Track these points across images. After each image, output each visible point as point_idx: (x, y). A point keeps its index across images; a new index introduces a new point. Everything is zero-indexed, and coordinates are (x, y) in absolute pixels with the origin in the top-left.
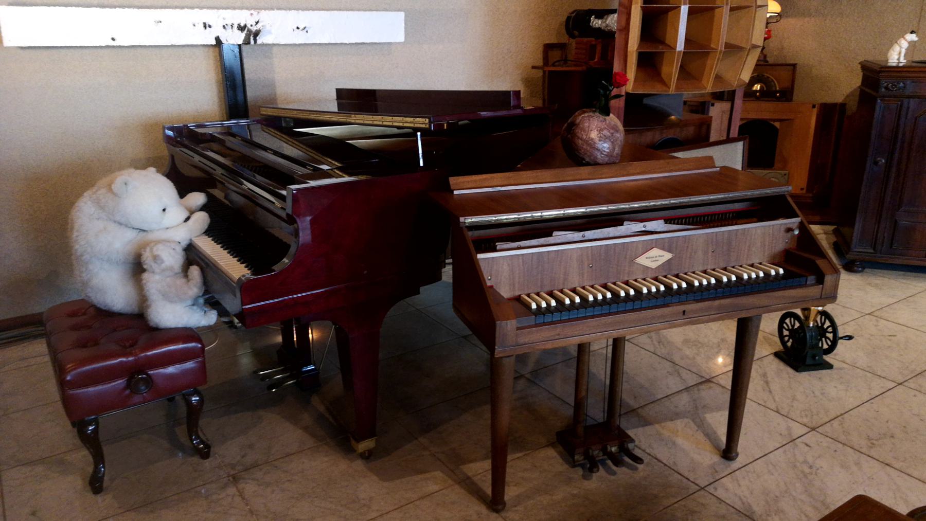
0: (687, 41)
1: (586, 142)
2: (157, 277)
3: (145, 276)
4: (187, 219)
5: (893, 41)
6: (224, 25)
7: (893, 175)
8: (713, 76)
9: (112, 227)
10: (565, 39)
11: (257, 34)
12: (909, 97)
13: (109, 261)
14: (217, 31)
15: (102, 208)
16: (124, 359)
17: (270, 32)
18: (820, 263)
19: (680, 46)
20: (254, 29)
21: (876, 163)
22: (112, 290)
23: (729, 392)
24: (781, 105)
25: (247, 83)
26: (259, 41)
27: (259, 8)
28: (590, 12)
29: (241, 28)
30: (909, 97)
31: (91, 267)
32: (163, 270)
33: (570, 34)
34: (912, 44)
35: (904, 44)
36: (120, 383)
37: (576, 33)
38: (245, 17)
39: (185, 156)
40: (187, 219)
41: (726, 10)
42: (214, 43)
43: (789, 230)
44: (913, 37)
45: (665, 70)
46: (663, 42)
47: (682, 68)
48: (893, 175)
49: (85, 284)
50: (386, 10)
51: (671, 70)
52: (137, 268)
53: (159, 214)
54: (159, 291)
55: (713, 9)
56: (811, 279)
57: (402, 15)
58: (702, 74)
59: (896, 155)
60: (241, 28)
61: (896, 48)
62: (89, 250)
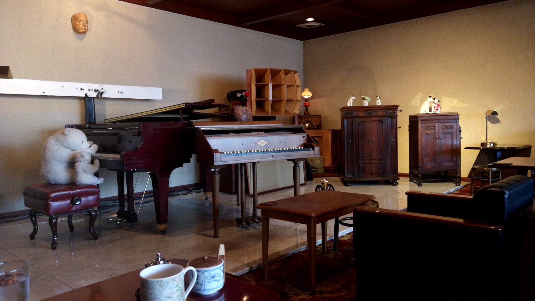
0: (273, 97)
1: (238, 114)
2: (82, 164)
3: (76, 164)
4: (90, 147)
5: (348, 99)
6: (88, 89)
7: (354, 146)
8: (284, 111)
9: (62, 148)
10: (227, 103)
11: (102, 93)
12: (355, 117)
13: (60, 161)
14: (86, 91)
15: (59, 141)
16: (72, 192)
17: (107, 93)
18: (313, 144)
19: (271, 98)
20: (101, 91)
21: (348, 142)
22: (59, 173)
23: (306, 234)
24: (318, 131)
25: (96, 114)
26: (103, 96)
27: (103, 83)
28: (236, 92)
29: (96, 91)
30: (355, 117)
31: (52, 164)
32: (85, 161)
33: (230, 101)
34: (353, 100)
35: (352, 100)
36: (68, 202)
37: (232, 99)
38: (97, 87)
39: (90, 126)
40: (90, 147)
41: (285, 86)
42: (84, 96)
43: (304, 137)
44: (353, 98)
45: (266, 107)
46: (265, 98)
47: (272, 107)
48: (354, 146)
49: (48, 172)
50: (155, 87)
51: (268, 107)
52: (72, 164)
53: (81, 144)
54: (82, 169)
55: (281, 85)
56: (311, 149)
57: (161, 89)
58: (280, 109)
59: (354, 139)
60: (96, 91)
61: (349, 102)
62: (53, 156)
